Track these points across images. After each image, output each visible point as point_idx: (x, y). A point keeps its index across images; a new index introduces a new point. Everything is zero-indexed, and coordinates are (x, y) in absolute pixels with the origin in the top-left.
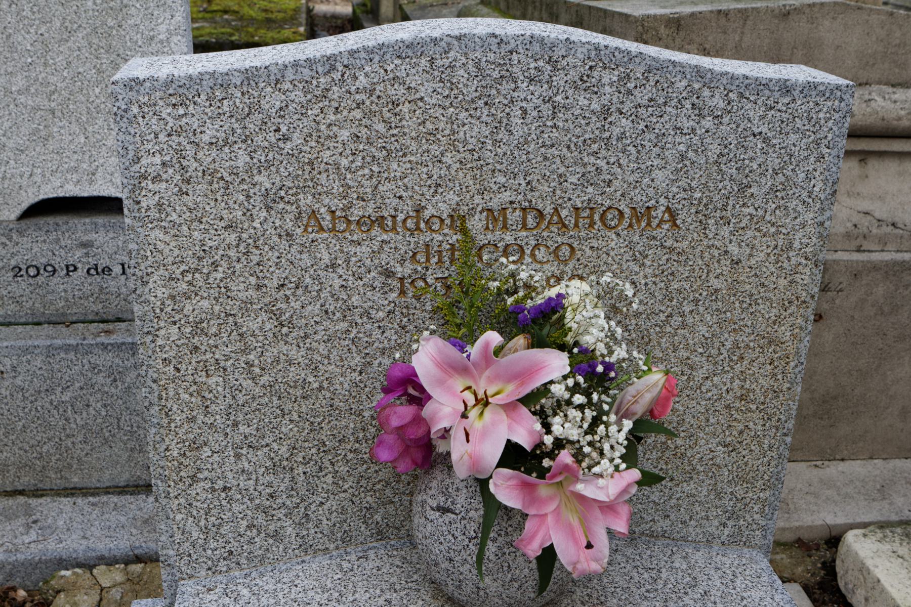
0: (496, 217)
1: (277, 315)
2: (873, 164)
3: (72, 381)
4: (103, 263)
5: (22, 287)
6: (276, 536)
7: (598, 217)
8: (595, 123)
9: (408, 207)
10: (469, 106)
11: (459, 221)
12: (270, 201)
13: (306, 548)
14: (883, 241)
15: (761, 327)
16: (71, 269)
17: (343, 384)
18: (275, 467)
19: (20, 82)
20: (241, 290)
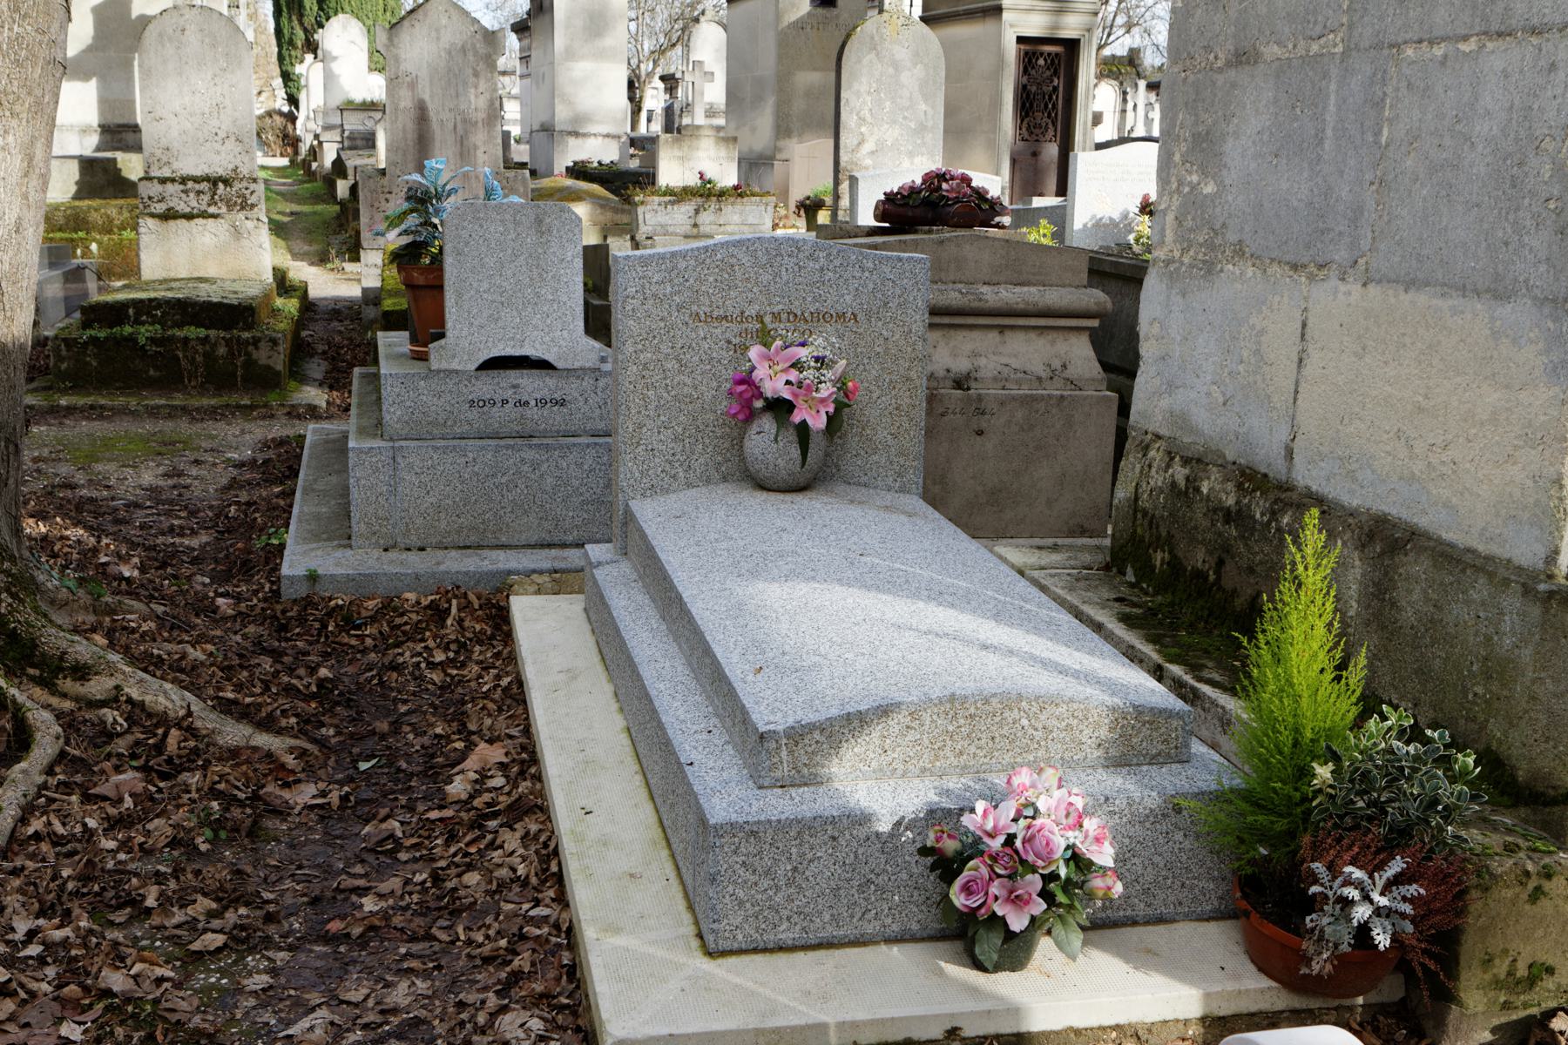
0: (776, 317)
1: (679, 361)
2: (1008, 333)
3: (508, 469)
4: (524, 399)
5: (473, 414)
6: (674, 477)
7: (821, 317)
8: (818, 274)
9: (737, 311)
10: (763, 267)
11: (760, 318)
12: (679, 308)
13: (689, 485)
14: (1019, 382)
15: (902, 372)
16: (505, 402)
17: (708, 396)
18: (676, 439)
19: (485, 285)
20: (665, 349)
